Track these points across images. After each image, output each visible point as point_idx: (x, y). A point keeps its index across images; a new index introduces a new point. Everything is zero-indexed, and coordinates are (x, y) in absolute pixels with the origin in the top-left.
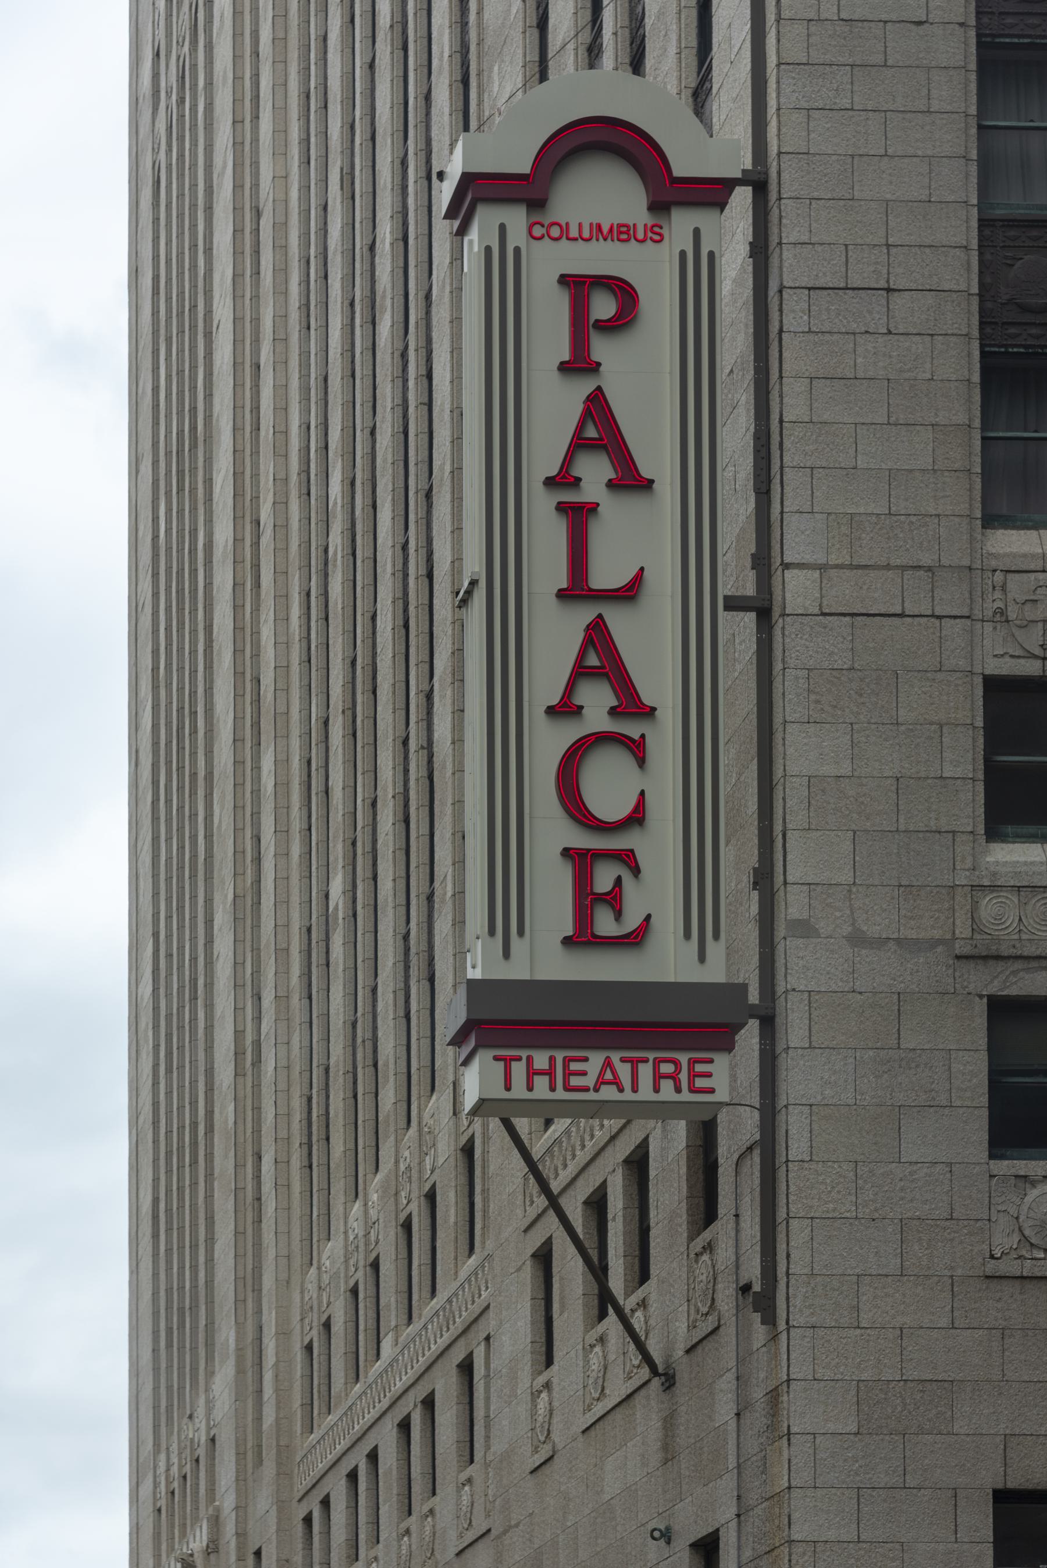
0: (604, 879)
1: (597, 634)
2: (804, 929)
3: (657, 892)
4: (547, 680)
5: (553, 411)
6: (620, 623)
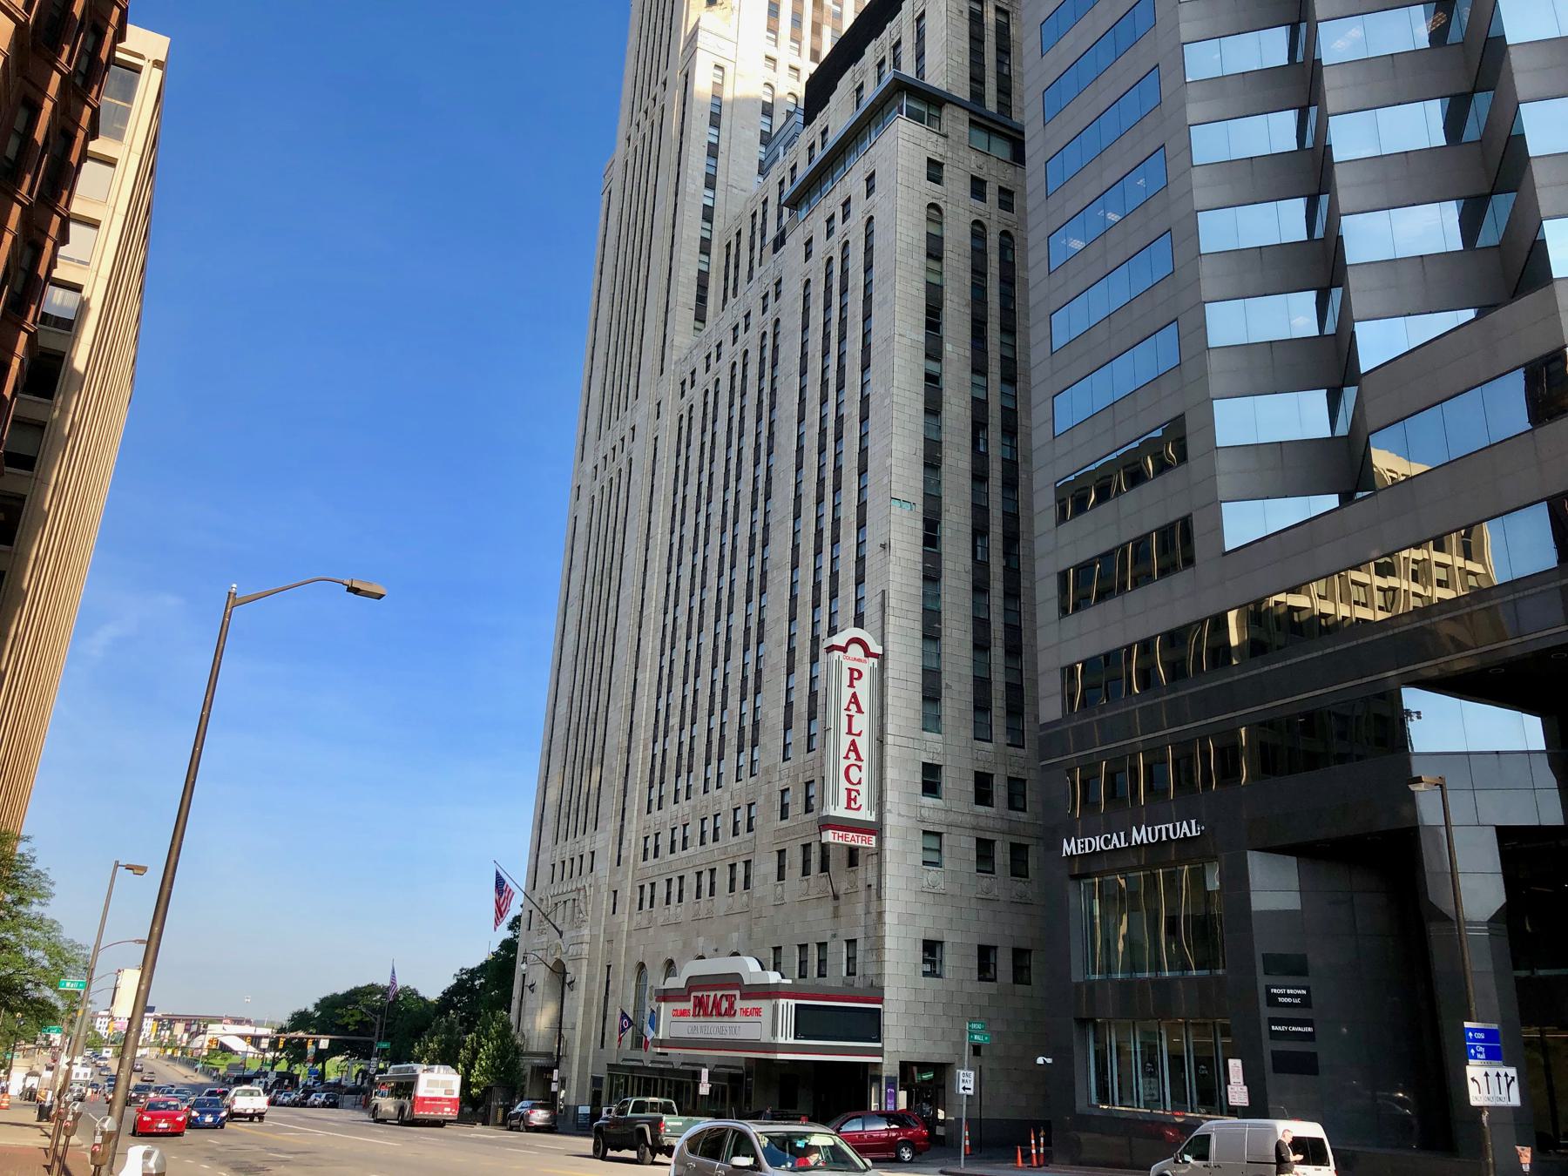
0: (853, 794)
1: (853, 743)
3: (862, 800)
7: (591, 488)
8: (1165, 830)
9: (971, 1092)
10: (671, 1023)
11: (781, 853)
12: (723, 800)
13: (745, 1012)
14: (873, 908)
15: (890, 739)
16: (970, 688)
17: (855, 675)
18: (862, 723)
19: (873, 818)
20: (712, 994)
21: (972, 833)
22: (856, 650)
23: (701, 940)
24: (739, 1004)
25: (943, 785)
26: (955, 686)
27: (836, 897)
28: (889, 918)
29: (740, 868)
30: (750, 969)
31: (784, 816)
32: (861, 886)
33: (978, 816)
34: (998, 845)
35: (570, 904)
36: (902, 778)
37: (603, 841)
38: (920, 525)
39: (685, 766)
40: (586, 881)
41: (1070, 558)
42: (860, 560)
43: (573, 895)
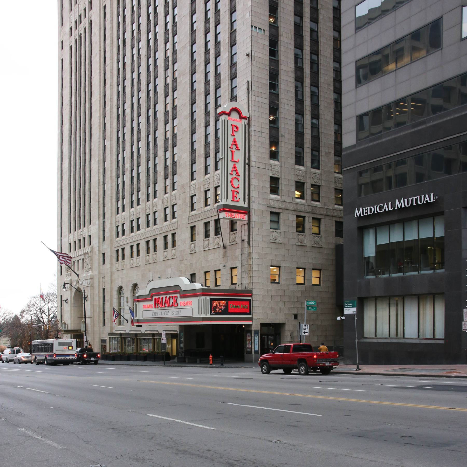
0: (235, 193)
1: (235, 167)
2: (254, 202)
3: (240, 196)
4: (230, 171)
5: (230, 139)
6: (237, 165)
7: (70, 42)
8: (416, 199)
9: (307, 334)
10: (145, 310)
11: (193, 228)
12: (158, 204)
13: (183, 304)
14: (246, 251)
15: (253, 164)
16: (293, 137)
17: (235, 129)
18: (239, 156)
19: (246, 205)
20: (164, 297)
21: (294, 213)
22: (235, 115)
23: (151, 273)
24: (179, 300)
25: (280, 188)
26: (286, 136)
27: (225, 247)
28: (254, 256)
29: (170, 238)
30: (185, 283)
31: (193, 209)
32: (238, 240)
33: (297, 204)
34: (307, 219)
35: (81, 261)
36: (260, 184)
37: (94, 229)
38: (267, 43)
39: (152, 181)
40: (88, 249)
41: (362, 52)
42: (233, 65)
43: (83, 257)
